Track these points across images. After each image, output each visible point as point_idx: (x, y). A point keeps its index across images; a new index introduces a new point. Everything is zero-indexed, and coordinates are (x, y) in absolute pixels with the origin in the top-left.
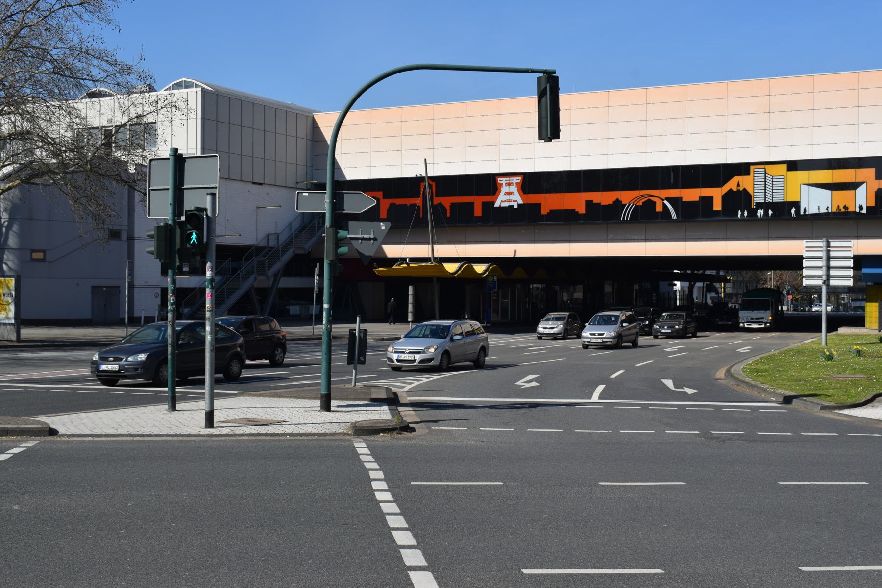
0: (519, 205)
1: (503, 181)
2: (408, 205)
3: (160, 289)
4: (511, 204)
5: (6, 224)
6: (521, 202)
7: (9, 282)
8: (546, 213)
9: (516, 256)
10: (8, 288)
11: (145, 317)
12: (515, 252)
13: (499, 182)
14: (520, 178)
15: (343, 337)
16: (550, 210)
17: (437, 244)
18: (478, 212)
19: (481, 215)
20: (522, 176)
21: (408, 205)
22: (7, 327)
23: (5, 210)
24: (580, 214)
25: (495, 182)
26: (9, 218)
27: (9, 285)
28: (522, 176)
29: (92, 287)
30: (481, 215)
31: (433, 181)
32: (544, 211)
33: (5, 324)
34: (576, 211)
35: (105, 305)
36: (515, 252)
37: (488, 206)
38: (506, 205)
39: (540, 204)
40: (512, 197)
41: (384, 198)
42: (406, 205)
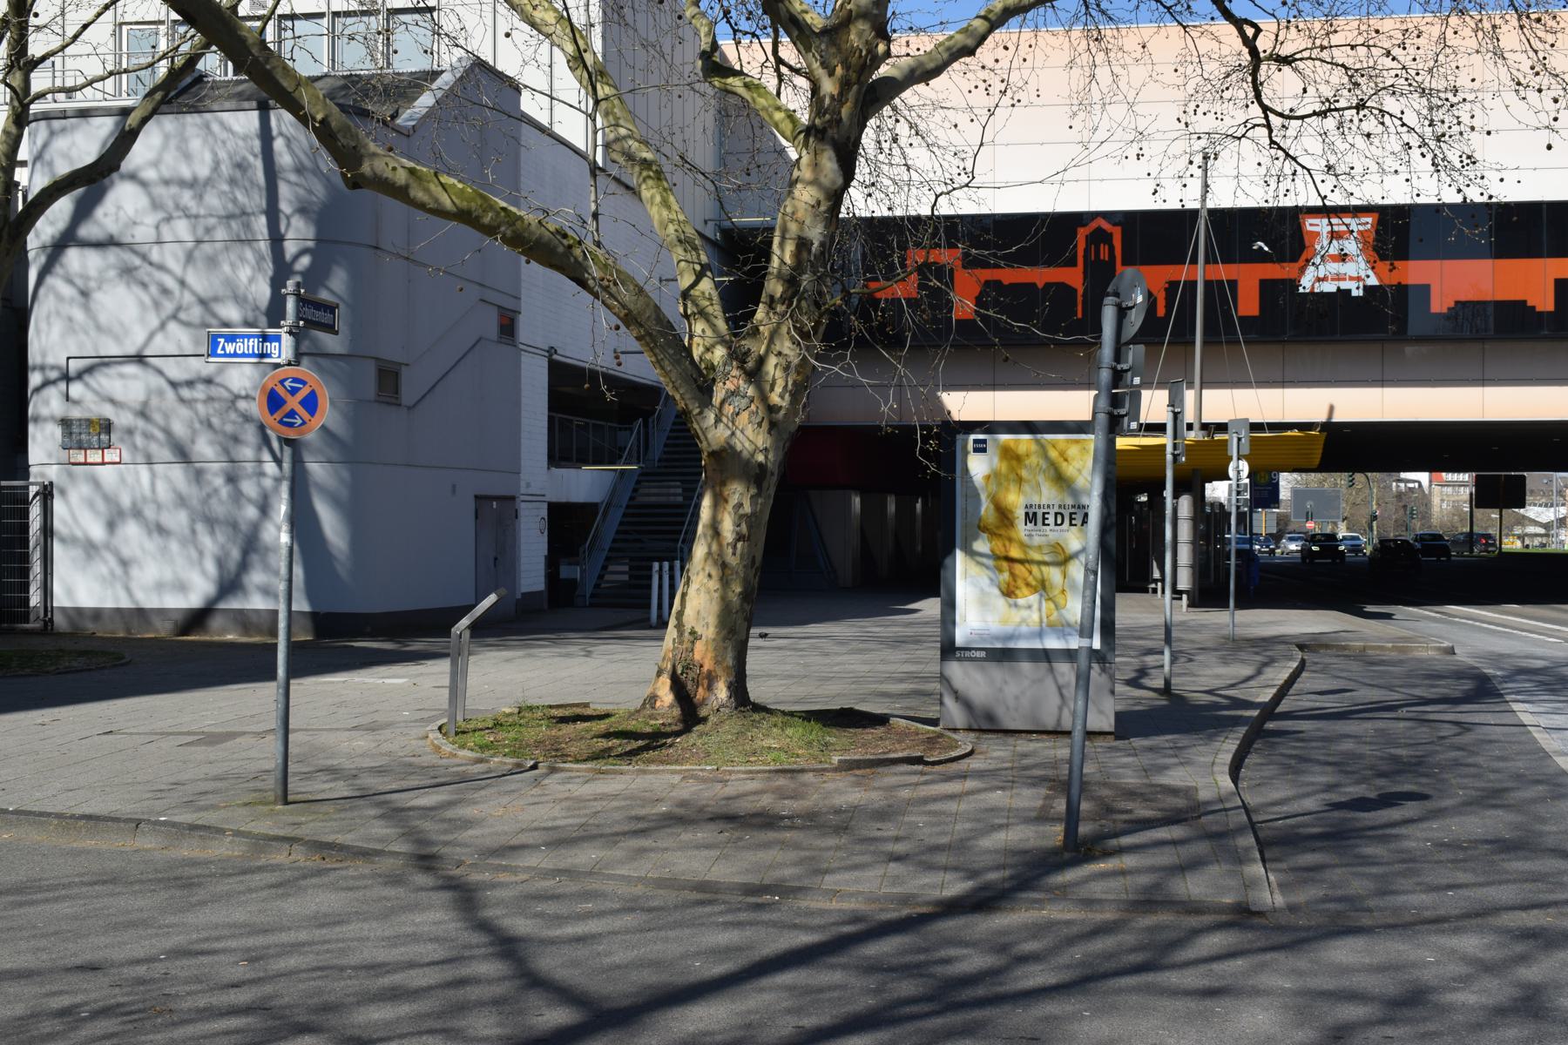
0: (1366, 288)
1: (1317, 226)
2: (1040, 286)
3: (546, 506)
4: (1344, 285)
5: (305, 261)
6: (1373, 281)
7: (1062, 454)
8: (1445, 311)
9: (1334, 420)
10: (1060, 480)
11: (1227, 606)
12: (1332, 409)
13: (1309, 228)
14: (1370, 220)
15: (1327, 646)
16: (1457, 303)
17: (1258, 387)
18: (1248, 304)
19: (1256, 313)
20: (1376, 215)
21: (1040, 286)
22: (1051, 670)
23: (302, 210)
24: (1541, 313)
25: (1298, 231)
26: (319, 240)
27: (1069, 470)
28: (1376, 215)
29: (476, 497)
30: (1256, 313)
31: (1115, 225)
32: (1440, 304)
33: (1046, 656)
34: (1529, 304)
35: (496, 559)
36: (1332, 409)
37: (1279, 294)
38: (1329, 287)
39: (1428, 287)
40: (1349, 268)
41: (964, 267)
42: (1033, 285)
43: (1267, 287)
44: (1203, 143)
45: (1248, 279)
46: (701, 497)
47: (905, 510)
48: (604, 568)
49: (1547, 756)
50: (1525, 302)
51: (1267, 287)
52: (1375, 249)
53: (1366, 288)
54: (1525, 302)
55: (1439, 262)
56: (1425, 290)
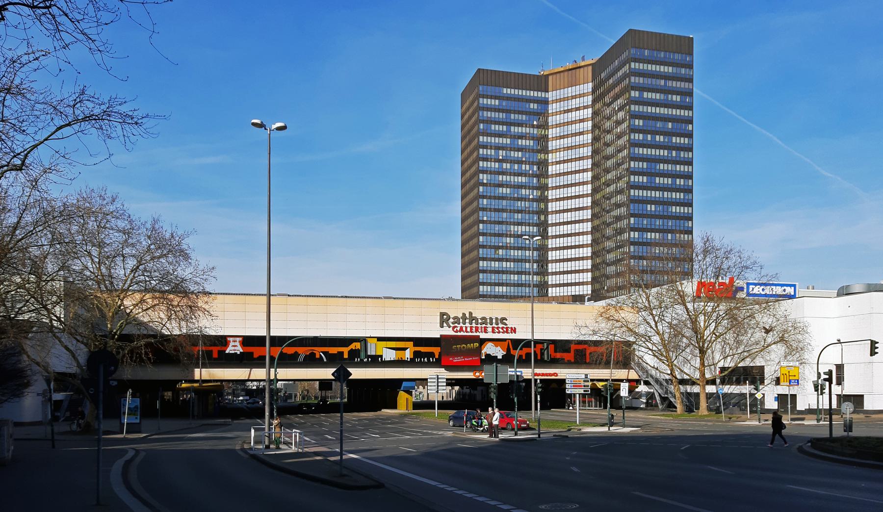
0: (240, 352)
6: (242, 351)
18: (215, 355)
24: (289, 354)
37: (222, 353)
38: (233, 352)
43: (219, 352)
44: (130, 241)
45: (215, 351)
46: (682, 450)
47: (643, 403)
48: (65, 413)
49: (726, 385)
50: (328, 352)
51: (219, 352)
52: (242, 344)
53: (240, 352)
54: (328, 352)
55: (385, 342)
56: (253, 353)
